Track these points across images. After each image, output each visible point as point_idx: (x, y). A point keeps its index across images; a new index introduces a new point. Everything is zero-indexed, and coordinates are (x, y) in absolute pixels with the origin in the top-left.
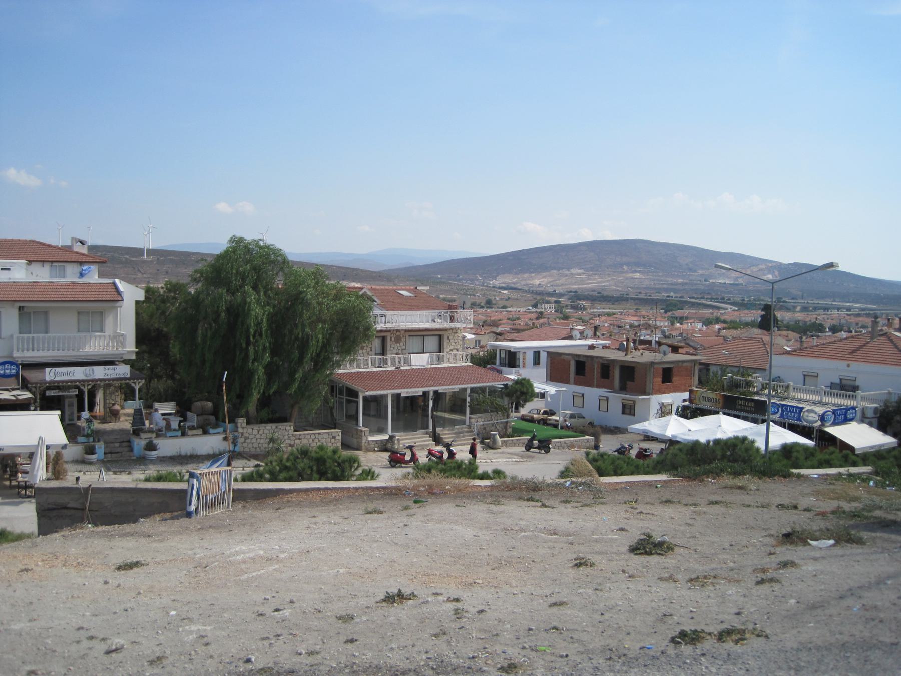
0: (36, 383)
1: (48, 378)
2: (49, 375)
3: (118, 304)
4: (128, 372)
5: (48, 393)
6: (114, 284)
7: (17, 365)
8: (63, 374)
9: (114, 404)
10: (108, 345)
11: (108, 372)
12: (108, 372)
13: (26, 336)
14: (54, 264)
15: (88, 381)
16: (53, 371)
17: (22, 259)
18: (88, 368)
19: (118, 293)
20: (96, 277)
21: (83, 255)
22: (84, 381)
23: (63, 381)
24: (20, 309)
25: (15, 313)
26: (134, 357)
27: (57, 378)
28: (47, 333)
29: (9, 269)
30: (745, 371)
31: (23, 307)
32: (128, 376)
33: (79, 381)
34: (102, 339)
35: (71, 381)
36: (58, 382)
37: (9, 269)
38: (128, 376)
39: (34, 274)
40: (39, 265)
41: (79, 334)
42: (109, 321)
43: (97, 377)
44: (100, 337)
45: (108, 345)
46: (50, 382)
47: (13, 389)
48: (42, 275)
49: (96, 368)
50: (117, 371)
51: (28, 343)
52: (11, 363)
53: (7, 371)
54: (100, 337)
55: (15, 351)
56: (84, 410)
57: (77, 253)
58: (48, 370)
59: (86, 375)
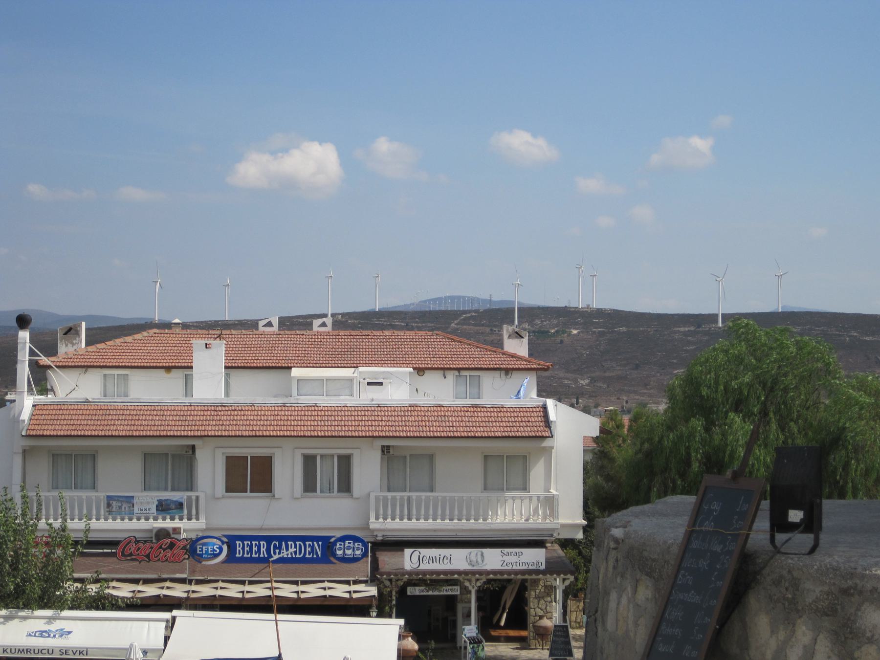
0: (389, 574)
1: (408, 566)
2: (411, 560)
3: (547, 443)
4: (543, 561)
5: (411, 591)
6: (545, 408)
7: (365, 544)
8: (433, 560)
9: (541, 617)
10: (536, 511)
11: (508, 559)
12: (508, 559)
13: (398, 494)
14: (464, 373)
15: (473, 573)
16: (416, 554)
17: (407, 365)
18: (474, 551)
19: (547, 423)
20: (534, 394)
21: (520, 358)
22: (466, 573)
23: (432, 572)
24: (385, 450)
25: (375, 456)
26: (580, 536)
27: (424, 566)
28: (432, 490)
29: (381, 384)
30: (52, 390)
31: (388, 447)
32: (543, 567)
33: (459, 573)
34: (518, 501)
35: (445, 572)
36: (425, 573)
37: (381, 384)
38: (543, 567)
39: (421, 393)
40: (436, 376)
41: (486, 494)
42: (537, 472)
43: (489, 567)
44: (514, 499)
45: (536, 511)
46: (410, 573)
47: (356, 582)
48: (399, 387)
49: (487, 552)
50: (523, 559)
51: (402, 506)
52: (356, 539)
53: (349, 552)
54: (514, 499)
55: (372, 520)
56: (470, 624)
57: (513, 356)
58: (408, 551)
59: (471, 563)
